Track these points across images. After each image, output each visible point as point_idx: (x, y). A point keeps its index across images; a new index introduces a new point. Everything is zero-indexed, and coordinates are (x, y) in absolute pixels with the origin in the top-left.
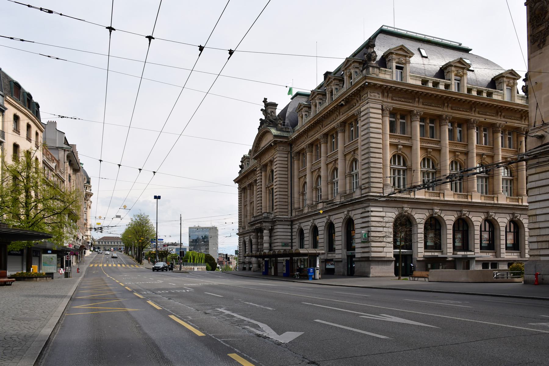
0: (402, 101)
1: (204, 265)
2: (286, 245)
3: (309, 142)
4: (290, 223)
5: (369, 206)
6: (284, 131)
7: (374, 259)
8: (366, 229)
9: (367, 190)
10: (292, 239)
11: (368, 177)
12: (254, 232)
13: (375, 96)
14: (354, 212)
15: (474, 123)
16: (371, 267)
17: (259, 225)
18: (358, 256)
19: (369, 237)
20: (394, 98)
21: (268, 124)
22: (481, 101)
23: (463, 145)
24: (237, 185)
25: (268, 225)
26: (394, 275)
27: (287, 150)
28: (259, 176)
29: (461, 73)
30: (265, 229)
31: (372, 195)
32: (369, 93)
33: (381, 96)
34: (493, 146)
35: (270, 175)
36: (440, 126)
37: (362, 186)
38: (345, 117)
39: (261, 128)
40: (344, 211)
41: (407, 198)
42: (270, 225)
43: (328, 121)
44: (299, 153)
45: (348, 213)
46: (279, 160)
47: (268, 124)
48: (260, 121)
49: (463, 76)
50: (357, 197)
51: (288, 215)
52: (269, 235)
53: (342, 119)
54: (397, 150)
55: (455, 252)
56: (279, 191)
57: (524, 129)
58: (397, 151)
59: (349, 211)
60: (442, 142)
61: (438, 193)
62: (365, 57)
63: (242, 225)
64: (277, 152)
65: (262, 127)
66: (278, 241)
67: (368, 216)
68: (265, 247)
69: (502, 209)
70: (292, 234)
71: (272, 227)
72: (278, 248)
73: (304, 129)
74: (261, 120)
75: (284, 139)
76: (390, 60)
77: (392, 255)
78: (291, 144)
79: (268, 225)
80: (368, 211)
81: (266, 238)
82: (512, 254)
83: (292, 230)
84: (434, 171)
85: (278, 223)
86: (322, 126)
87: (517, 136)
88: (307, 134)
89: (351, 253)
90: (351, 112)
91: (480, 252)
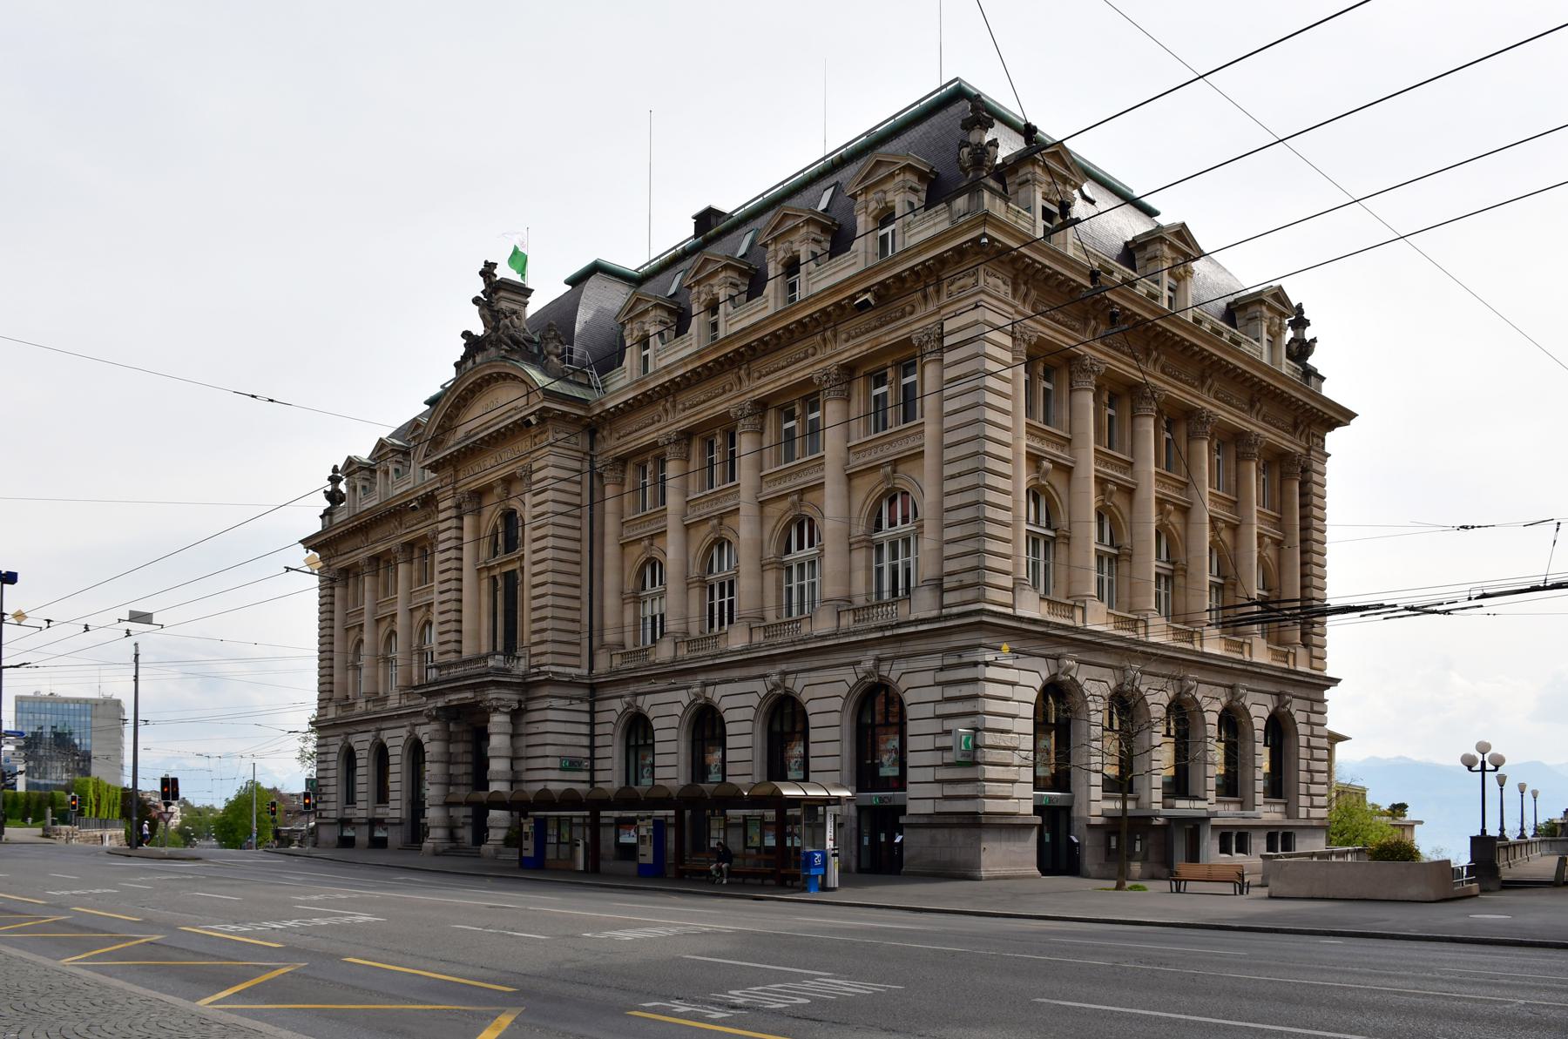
0: (1057, 322)
1: (120, 827)
2: (573, 765)
3: (683, 425)
5: (980, 646)
6: (570, 382)
7: (992, 821)
8: (967, 721)
9: (969, 594)
10: (592, 747)
11: (977, 552)
12: (432, 719)
15: (1207, 422)
16: (983, 845)
17: (469, 695)
18: (913, 808)
19: (976, 747)
21: (506, 351)
22: (1230, 360)
23: (1178, 485)
25: (510, 697)
26: (1037, 872)
27: (579, 447)
28: (449, 528)
30: (496, 709)
31: (992, 612)
32: (981, 273)
33: (1010, 291)
34: (1237, 496)
35: (496, 526)
36: (1133, 418)
37: (946, 579)
38: (864, 348)
39: (470, 363)
42: (516, 697)
43: (780, 358)
44: (622, 461)
45: (876, 667)
47: (506, 351)
48: (465, 341)
49: (1184, 278)
50: (922, 615)
51: (579, 667)
52: (510, 731)
53: (846, 355)
54: (1036, 475)
55: (1169, 801)
56: (554, 583)
57: (1299, 460)
58: (1038, 479)
59: (879, 660)
60: (1138, 467)
61: (1133, 620)
62: (965, 154)
63: (337, 694)
65: (478, 359)
66: (549, 750)
67: (975, 680)
68: (497, 772)
69: (1258, 679)
70: (592, 730)
71: (520, 702)
73: (667, 379)
74: (466, 334)
75: (574, 407)
76: (1028, 181)
77: (1027, 808)
78: (593, 427)
80: (976, 664)
81: (498, 742)
82: (1272, 808)
83: (592, 718)
85: (545, 691)
86: (748, 375)
87: (1281, 477)
88: (674, 397)
89: (880, 798)
90: (890, 333)
91: (1218, 801)
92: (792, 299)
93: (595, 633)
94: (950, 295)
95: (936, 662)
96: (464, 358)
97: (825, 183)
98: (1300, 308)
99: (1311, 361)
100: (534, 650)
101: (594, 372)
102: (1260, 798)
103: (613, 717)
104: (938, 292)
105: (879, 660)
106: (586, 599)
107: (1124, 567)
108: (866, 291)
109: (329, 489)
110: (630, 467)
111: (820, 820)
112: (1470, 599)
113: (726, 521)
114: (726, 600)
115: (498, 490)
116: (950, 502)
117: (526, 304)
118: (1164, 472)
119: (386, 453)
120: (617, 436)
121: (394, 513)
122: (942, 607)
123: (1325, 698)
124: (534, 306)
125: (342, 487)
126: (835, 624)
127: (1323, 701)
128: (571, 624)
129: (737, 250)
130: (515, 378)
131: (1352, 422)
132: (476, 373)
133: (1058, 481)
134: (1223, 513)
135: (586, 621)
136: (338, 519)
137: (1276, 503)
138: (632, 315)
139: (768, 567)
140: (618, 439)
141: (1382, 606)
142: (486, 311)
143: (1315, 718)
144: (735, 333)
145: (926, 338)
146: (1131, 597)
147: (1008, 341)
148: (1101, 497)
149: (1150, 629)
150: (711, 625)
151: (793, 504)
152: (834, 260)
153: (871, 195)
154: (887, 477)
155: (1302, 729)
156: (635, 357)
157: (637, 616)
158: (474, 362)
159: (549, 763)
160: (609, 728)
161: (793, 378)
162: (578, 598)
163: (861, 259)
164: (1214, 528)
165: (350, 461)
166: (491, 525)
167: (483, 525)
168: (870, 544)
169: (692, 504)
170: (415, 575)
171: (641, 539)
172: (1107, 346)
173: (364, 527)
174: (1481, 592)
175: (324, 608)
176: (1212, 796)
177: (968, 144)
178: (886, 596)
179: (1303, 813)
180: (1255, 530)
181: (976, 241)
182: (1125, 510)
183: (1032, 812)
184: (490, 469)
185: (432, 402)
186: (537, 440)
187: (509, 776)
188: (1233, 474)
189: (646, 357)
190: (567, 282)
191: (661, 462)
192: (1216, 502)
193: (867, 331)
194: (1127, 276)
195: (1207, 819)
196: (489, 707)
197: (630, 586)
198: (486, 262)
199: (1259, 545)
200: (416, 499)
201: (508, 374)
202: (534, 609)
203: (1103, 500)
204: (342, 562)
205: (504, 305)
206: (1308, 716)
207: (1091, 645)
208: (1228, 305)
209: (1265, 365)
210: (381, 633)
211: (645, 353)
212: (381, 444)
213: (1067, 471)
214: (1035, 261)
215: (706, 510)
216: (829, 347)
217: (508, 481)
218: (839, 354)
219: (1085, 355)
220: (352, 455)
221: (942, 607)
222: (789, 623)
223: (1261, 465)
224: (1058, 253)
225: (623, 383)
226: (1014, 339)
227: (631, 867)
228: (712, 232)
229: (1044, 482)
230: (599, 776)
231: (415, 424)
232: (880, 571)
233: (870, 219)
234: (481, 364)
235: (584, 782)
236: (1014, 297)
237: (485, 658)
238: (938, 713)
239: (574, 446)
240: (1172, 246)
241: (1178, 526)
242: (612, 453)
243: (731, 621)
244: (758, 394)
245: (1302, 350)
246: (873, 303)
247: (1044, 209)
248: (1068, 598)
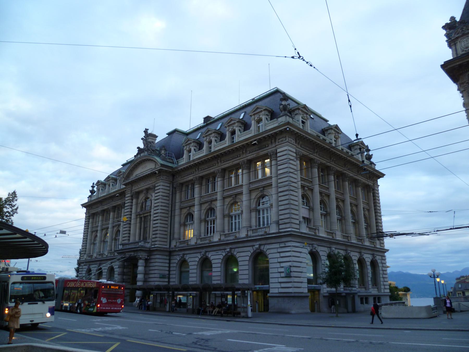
2: (163, 276)
4: (167, 253)
10: (169, 271)
13: (291, 141)
14: (267, 247)
20: (303, 146)
24: (84, 210)
26: (309, 311)
28: (128, 203)
29: (337, 136)
30: (141, 259)
33: (294, 142)
37: (280, 221)
38: (254, 155)
40: (255, 244)
41: (310, 234)
44: (182, 184)
46: (162, 189)
48: (138, 150)
49: (338, 138)
52: (145, 265)
54: (303, 191)
64: (161, 180)
66: (156, 272)
70: (170, 265)
72: (155, 281)
74: (138, 148)
76: (297, 114)
77: (306, 291)
79: (143, 255)
81: (141, 269)
84: (325, 213)
85: (155, 253)
86: (221, 161)
90: (262, 151)
92: (233, 142)
93: (172, 235)
94: (279, 142)
95: (277, 246)
96: (137, 154)
97: (241, 111)
98: (367, 146)
99: (372, 160)
100: (153, 240)
101: (175, 159)
102: (370, 286)
103: (176, 261)
104: (275, 141)
105: (260, 245)
106: (169, 225)
107: (328, 217)
108: (255, 140)
109: (91, 189)
110: (184, 186)
111: (246, 295)
112: (434, 231)
113: (213, 203)
114: (212, 226)
115: (145, 192)
116: (280, 199)
117: (156, 140)
118: (337, 190)
119: (110, 180)
120: (181, 177)
121: (111, 197)
122: (279, 229)
123: (385, 255)
124: (158, 140)
125: (95, 189)
127: (385, 256)
128: (165, 232)
129: (217, 128)
130: (152, 160)
131: (384, 176)
132: (141, 158)
133: (309, 193)
134: (354, 202)
135: (169, 231)
136: (93, 199)
137: (367, 198)
138: (186, 144)
140: (181, 178)
141: (413, 233)
142: (145, 142)
143: (383, 261)
144: (217, 150)
145: (272, 153)
146: (330, 226)
147: (295, 155)
148: (321, 197)
149: (352, 239)
150: (208, 233)
152: (245, 132)
153: (256, 116)
155: (380, 265)
156: (187, 156)
158: (140, 156)
159: (156, 275)
160: (175, 265)
162: (167, 224)
163: (253, 132)
164: (351, 206)
165: (98, 182)
169: (203, 197)
170: (116, 216)
171: (187, 207)
172: (320, 156)
173: (100, 202)
174: (437, 230)
175: (86, 225)
176: (357, 286)
177: (282, 105)
178: (261, 226)
179: (382, 291)
180: (362, 207)
181: (286, 129)
182: (327, 201)
183: (307, 292)
184: (143, 186)
185: (123, 165)
186: (158, 178)
187: (143, 280)
188: (355, 191)
189: (190, 156)
190: (167, 134)
191: (193, 185)
192: (351, 199)
193: (255, 151)
194: (324, 138)
195: (356, 293)
196: (139, 258)
197: (183, 221)
198: (146, 129)
199: (363, 211)
200: (118, 193)
201: (150, 159)
202: (154, 228)
203: (321, 198)
204: (93, 211)
205: (150, 140)
206: (381, 261)
207: (322, 241)
208: (349, 145)
209: (301, 129)
210: (103, 234)
211: (190, 154)
212: (108, 177)
213: (312, 190)
214: (301, 134)
215: (207, 199)
216: (244, 155)
217: (148, 190)
218: (247, 157)
219: (315, 159)
220: (99, 180)
221: (279, 229)
222: (232, 233)
223: (349, 182)
224: (306, 132)
225: (183, 161)
226: (296, 154)
227: (184, 310)
228: (209, 122)
229: (305, 193)
230: (171, 280)
231: (119, 172)
232: (259, 218)
233: (255, 122)
234: (142, 156)
235: (166, 282)
236: (296, 143)
237: (138, 243)
238: (279, 261)
239: (168, 180)
240: (334, 130)
241: (341, 205)
242: (179, 182)
243: (214, 232)
244: (223, 167)
245: (369, 157)
246: (257, 143)
247: (302, 121)
248: (314, 226)
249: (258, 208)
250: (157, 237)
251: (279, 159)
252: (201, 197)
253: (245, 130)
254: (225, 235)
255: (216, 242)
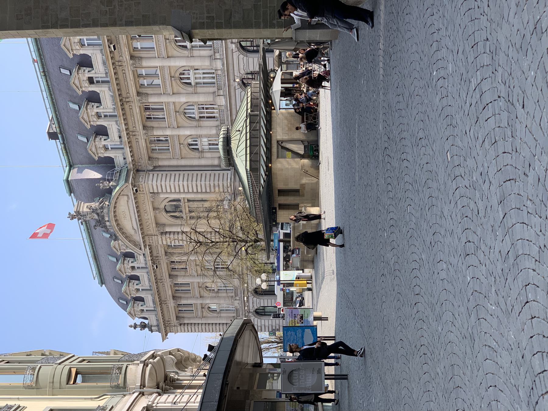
27: (145, 175)
120: (141, 159)
126: (219, 60)
139: (196, 91)
150: (214, 117)
151: (175, 80)
154: (170, 42)
157: (209, 152)
161: (132, 79)
166: (170, 219)
167: (170, 223)
168: (191, 50)
204: (174, 321)
216: (124, 64)
249: (197, 118)
250: (218, 184)
251: (160, 191)
252: (169, 127)
253: (107, 135)
254: (235, 296)
255: (226, 101)
